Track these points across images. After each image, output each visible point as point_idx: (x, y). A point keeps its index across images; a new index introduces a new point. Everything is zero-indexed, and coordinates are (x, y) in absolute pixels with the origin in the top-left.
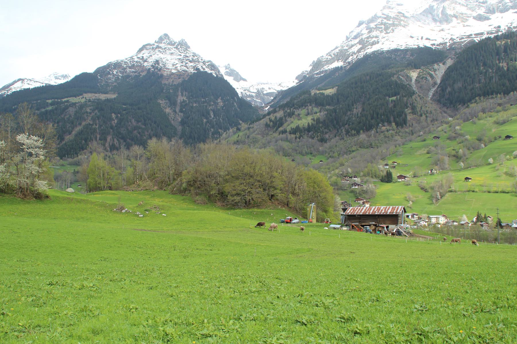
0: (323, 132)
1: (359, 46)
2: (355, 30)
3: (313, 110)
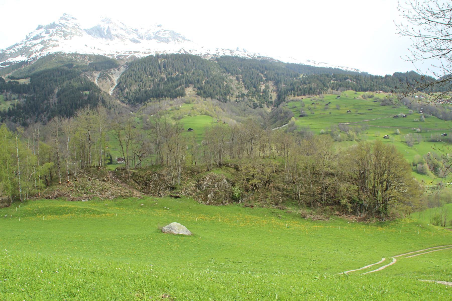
0: (24, 117)
1: (42, 46)
2: (34, 32)
3: (11, 96)
